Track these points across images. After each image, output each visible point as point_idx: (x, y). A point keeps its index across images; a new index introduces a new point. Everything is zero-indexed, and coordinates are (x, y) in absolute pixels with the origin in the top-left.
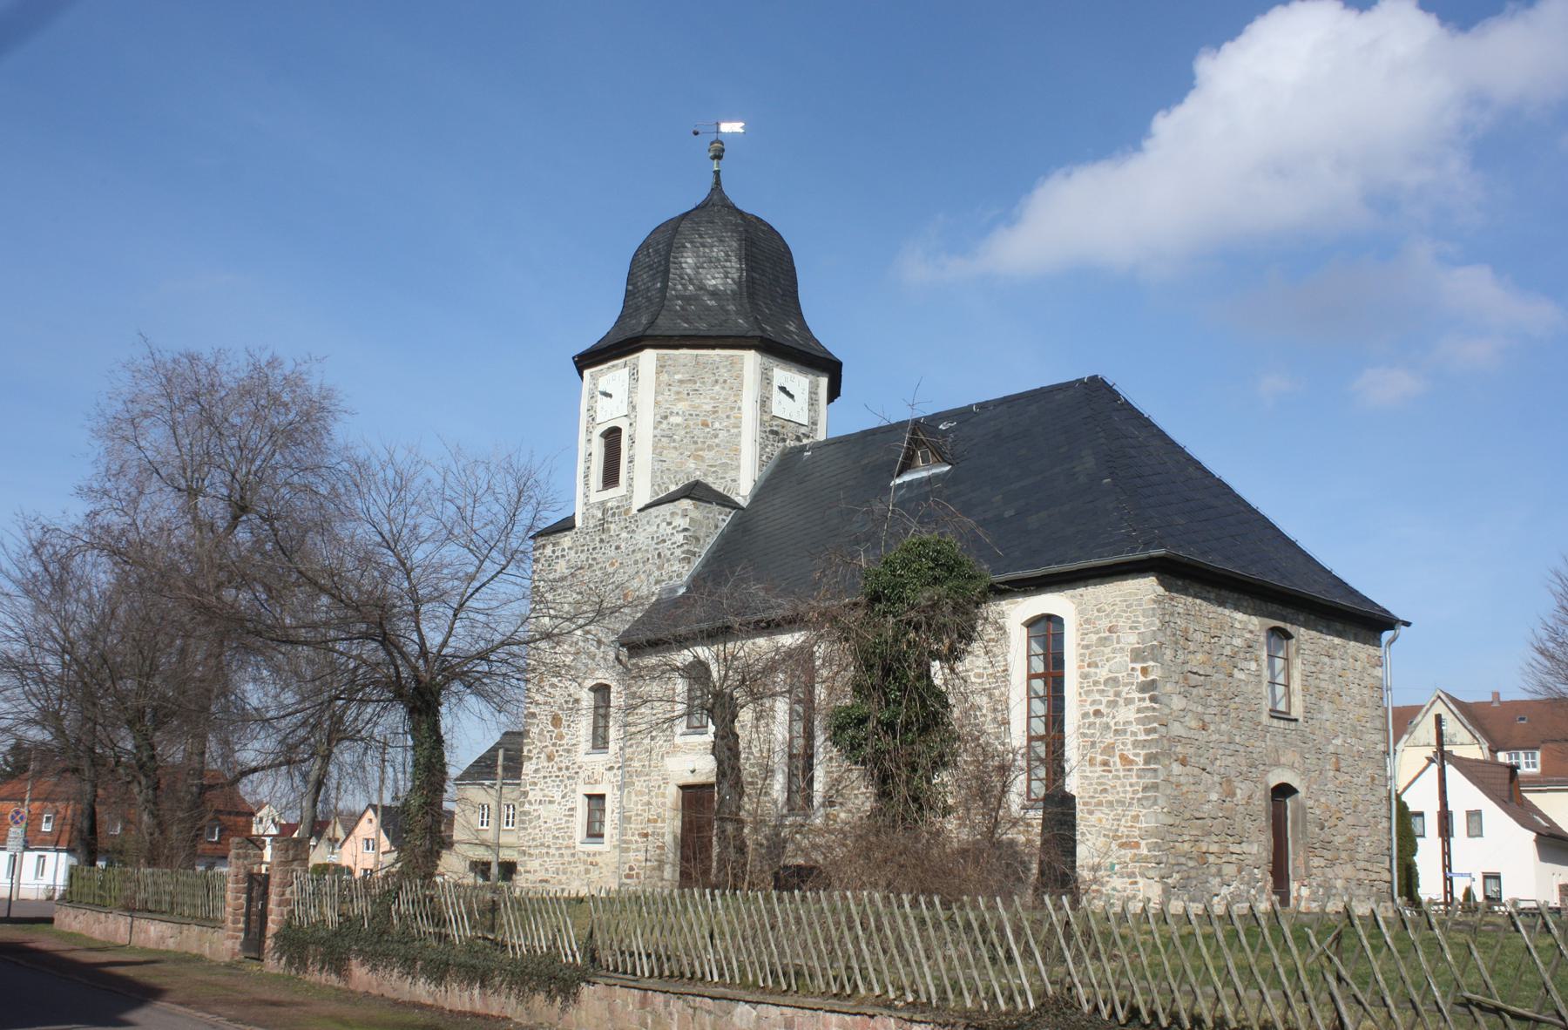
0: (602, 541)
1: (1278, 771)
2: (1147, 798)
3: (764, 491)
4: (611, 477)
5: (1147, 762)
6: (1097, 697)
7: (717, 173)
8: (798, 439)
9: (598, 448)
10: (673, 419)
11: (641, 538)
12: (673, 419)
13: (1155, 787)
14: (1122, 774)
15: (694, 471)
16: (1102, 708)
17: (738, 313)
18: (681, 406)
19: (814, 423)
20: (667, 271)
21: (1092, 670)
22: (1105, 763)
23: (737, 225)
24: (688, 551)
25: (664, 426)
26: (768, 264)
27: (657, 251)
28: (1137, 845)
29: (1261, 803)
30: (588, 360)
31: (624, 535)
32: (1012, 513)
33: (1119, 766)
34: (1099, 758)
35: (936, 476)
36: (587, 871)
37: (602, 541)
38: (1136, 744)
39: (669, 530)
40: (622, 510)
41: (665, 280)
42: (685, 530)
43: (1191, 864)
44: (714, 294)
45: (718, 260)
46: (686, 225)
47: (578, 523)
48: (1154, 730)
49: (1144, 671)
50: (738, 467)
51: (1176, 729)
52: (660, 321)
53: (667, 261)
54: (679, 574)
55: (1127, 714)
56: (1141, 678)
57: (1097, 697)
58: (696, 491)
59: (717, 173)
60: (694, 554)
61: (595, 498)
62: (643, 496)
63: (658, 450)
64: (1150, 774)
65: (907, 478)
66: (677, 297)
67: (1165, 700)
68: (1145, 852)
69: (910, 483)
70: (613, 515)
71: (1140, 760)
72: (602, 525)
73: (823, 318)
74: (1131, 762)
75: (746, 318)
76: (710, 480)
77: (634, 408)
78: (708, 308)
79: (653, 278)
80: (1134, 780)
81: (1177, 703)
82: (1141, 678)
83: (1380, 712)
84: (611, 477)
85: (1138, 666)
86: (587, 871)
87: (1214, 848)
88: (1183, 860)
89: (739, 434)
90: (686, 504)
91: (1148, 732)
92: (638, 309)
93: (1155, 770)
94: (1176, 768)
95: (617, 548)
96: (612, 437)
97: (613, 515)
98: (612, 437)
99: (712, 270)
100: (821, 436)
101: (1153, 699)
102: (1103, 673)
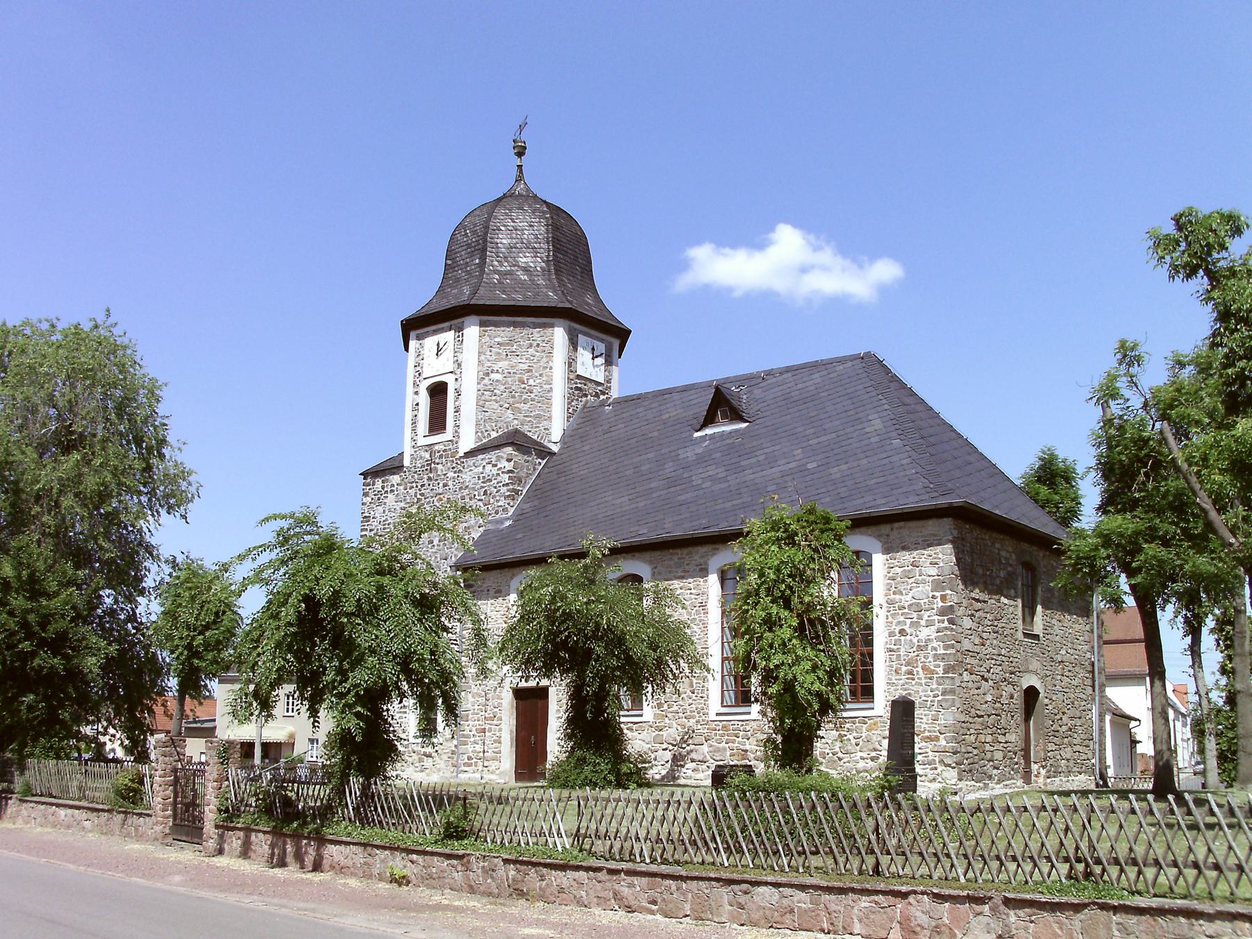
0: (430, 479)
1: (1027, 676)
2: (946, 700)
3: (567, 438)
4: (437, 422)
5: (946, 672)
6: (902, 619)
7: (520, 167)
8: (597, 395)
9: (424, 399)
10: (494, 376)
11: (467, 477)
12: (494, 376)
13: (952, 692)
14: (923, 681)
15: (511, 421)
16: (906, 628)
17: (546, 287)
18: (503, 364)
19: (609, 381)
20: (484, 250)
21: (897, 597)
22: (910, 673)
23: (544, 212)
24: (514, 490)
25: (486, 381)
26: (569, 247)
27: (474, 232)
28: (937, 739)
29: (1018, 700)
30: (415, 326)
31: (451, 474)
32: (814, 465)
33: (921, 674)
34: (904, 669)
35: (736, 431)
36: (420, 760)
37: (430, 479)
38: (936, 657)
39: (494, 471)
40: (449, 452)
41: (483, 259)
42: (510, 471)
43: (975, 752)
44: (526, 270)
45: (529, 242)
46: (500, 212)
47: (407, 462)
48: (952, 646)
49: (943, 598)
50: (550, 418)
51: (966, 645)
52: (482, 291)
53: (485, 241)
54: (505, 511)
55: (930, 632)
56: (941, 604)
57: (902, 619)
58: (517, 441)
59: (520, 167)
60: (517, 492)
61: (422, 441)
62: (467, 442)
63: (481, 406)
64: (947, 681)
65: (709, 431)
66: (495, 272)
67: (959, 621)
68: (943, 743)
69: (712, 437)
70: (441, 457)
71: (940, 670)
72: (430, 466)
73: (614, 292)
74: (932, 672)
75: (555, 291)
76: (525, 429)
77: (459, 365)
78: (522, 283)
79: (472, 255)
80: (934, 686)
81: (967, 623)
82: (941, 604)
83: (1088, 627)
84: (437, 422)
85: (938, 594)
86: (420, 760)
87: (989, 739)
88: (970, 749)
89: (550, 390)
90: (509, 450)
91: (946, 647)
92: (457, 280)
93: (953, 678)
94: (966, 676)
95: (445, 485)
96: (438, 392)
97: (441, 457)
98: (438, 392)
99: (521, 253)
100: (615, 393)
101: (951, 621)
102: (907, 599)
